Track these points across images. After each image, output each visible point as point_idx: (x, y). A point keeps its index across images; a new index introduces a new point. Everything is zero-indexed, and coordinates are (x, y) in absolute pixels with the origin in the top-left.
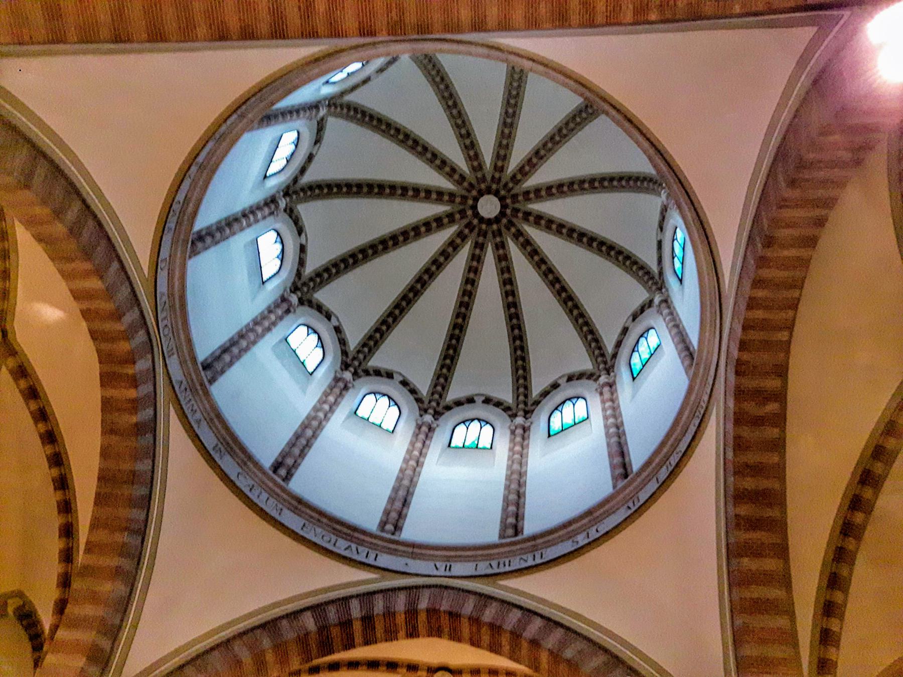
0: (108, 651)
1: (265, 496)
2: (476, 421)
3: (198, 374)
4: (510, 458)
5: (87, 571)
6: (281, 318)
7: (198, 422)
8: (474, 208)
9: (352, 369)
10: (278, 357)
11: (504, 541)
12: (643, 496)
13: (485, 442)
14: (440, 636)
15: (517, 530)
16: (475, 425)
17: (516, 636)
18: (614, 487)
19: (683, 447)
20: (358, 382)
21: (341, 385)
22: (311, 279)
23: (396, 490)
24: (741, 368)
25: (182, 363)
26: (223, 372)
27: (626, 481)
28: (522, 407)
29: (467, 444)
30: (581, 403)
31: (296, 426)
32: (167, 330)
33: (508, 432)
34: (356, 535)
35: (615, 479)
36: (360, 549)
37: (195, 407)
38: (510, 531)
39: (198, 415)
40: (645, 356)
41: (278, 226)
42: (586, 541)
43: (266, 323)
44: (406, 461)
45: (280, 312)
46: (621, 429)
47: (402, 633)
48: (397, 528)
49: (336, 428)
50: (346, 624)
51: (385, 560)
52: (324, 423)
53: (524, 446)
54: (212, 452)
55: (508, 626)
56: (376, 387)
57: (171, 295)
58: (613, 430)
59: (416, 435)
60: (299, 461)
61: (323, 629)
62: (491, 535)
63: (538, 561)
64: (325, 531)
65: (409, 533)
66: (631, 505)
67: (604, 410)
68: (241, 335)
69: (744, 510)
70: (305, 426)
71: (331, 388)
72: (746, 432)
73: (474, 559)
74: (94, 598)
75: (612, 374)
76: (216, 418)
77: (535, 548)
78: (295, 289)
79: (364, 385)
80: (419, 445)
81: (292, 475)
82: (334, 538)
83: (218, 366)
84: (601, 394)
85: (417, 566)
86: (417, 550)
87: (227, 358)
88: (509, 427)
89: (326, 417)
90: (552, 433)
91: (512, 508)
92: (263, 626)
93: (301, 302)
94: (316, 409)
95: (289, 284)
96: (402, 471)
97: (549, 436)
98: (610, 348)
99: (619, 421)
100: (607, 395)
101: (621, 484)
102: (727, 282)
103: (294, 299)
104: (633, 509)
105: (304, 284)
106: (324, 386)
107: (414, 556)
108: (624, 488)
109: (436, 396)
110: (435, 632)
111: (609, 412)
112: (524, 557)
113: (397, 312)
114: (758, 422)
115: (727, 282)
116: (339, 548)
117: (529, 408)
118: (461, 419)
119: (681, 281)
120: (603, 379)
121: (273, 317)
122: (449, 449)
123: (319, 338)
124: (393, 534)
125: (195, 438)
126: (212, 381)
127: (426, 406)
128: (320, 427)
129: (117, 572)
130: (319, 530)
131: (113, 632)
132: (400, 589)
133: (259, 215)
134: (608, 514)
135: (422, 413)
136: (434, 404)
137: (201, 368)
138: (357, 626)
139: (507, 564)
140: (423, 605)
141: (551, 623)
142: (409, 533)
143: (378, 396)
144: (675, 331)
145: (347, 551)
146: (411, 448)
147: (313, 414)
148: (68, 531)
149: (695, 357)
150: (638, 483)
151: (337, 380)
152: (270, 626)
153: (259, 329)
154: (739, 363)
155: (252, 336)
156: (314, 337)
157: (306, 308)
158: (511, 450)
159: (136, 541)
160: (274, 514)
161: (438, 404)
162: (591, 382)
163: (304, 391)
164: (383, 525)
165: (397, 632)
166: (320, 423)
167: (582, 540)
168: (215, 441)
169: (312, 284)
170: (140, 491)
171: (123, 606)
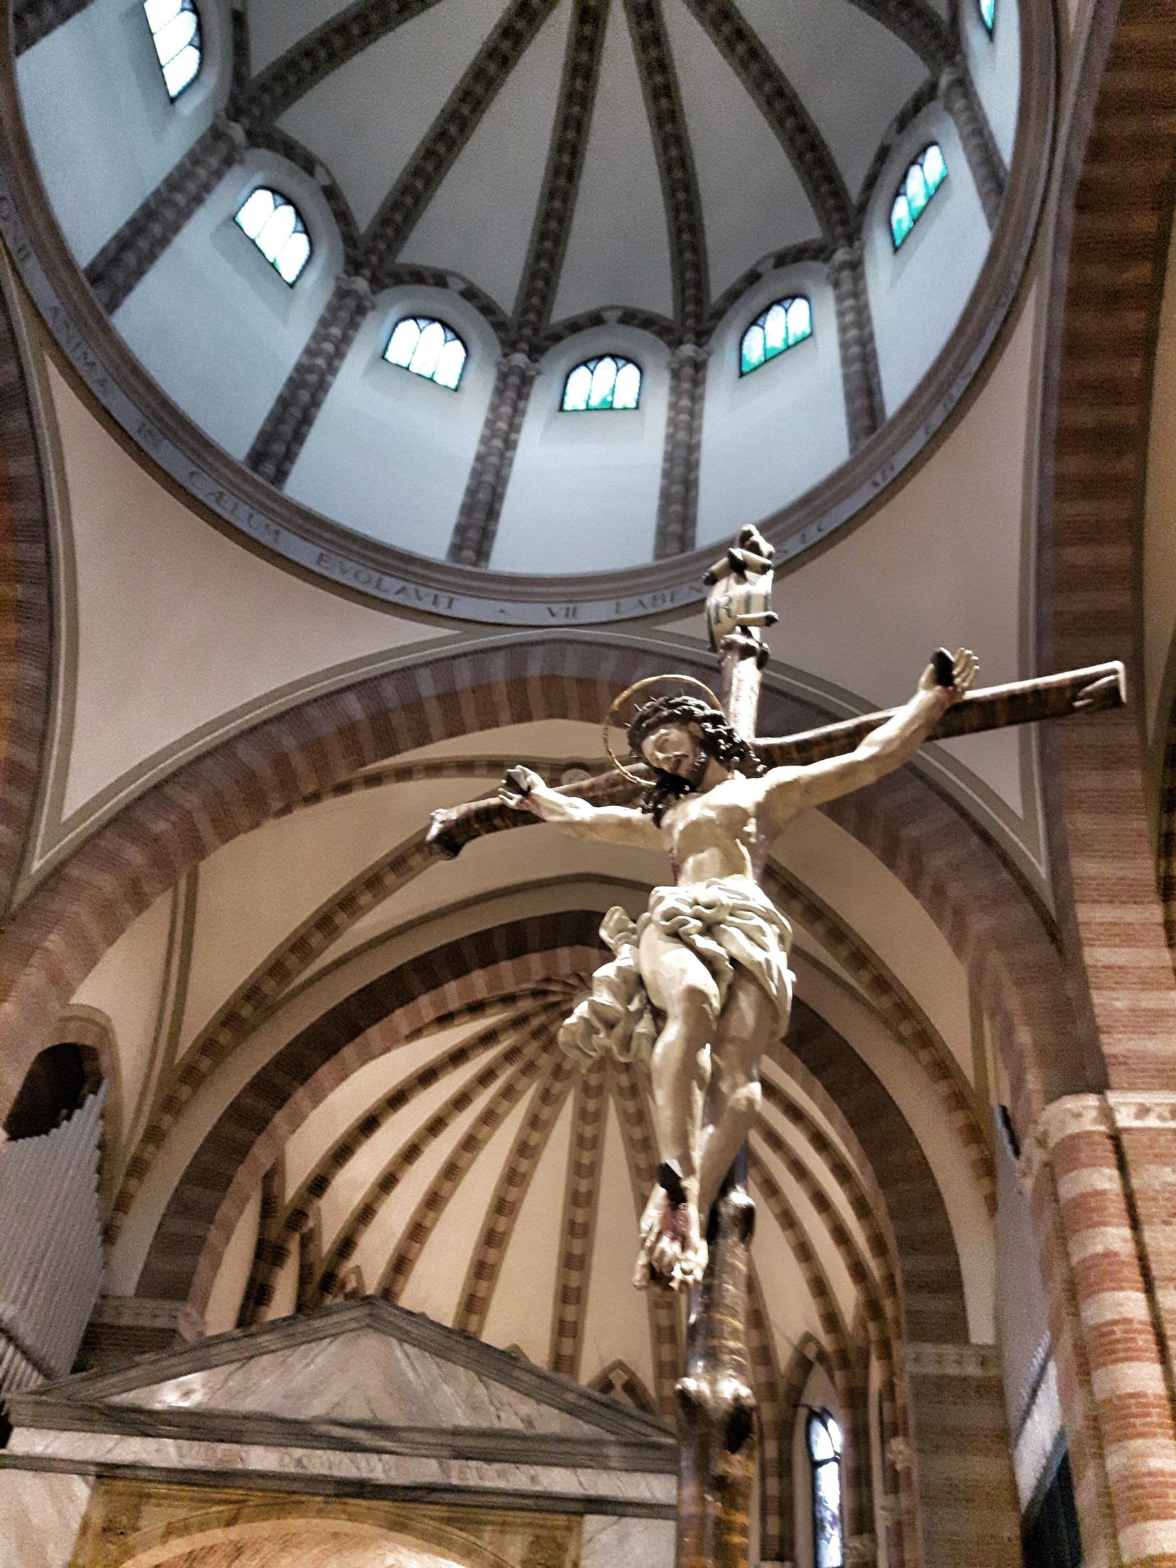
0: (35, 769)
3: (84, 293)
6: (218, 175)
9: (367, 272)
11: (661, 562)
12: (902, 460)
13: (626, 396)
14: (564, 716)
15: (685, 540)
16: (607, 364)
18: (853, 450)
20: (383, 296)
21: (350, 303)
22: (264, 88)
23: (471, 492)
24: (1088, 198)
25: (50, 272)
26: (128, 289)
27: (873, 436)
28: (689, 325)
29: (594, 403)
30: (800, 305)
34: (411, 568)
35: (855, 435)
36: (423, 591)
38: (674, 546)
40: (920, 202)
42: (801, 547)
43: (192, 187)
44: (485, 440)
45: (214, 162)
46: (869, 348)
47: (505, 715)
48: (483, 554)
50: (414, 706)
51: (466, 607)
53: (696, 398)
56: (418, 305)
58: (855, 350)
59: (499, 392)
62: (636, 548)
64: (351, 563)
66: (878, 477)
67: (840, 314)
69: (1075, 464)
75: (857, 244)
78: (235, 111)
79: (395, 302)
80: (506, 410)
82: (376, 576)
84: (836, 285)
85: (516, 612)
87: (130, 258)
88: (669, 365)
89: (332, 370)
91: (676, 508)
95: (222, 104)
96: (479, 458)
97: (742, 375)
98: (854, 185)
99: (866, 331)
100: (847, 286)
101: (866, 442)
103: (237, 132)
105: (253, 100)
107: (513, 598)
108: (870, 449)
109: (532, 316)
111: (849, 318)
113: (441, 149)
114: (1113, 299)
116: (386, 591)
117: (708, 325)
118: (577, 356)
119: (990, 33)
120: (841, 255)
121: (202, 172)
122: (561, 415)
123: (299, 214)
124: (475, 565)
126: (113, 305)
127: (513, 336)
128: (322, 387)
130: (349, 565)
131: (42, 740)
134: (848, 493)
135: (507, 351)
136: (527, 331)
137: (87, 285)
138: (433, 710)
139: (668, 599)
144: (975, 141)
145: (401, 595)
147: (306, 361)
149: (1006, 189)
151: (341, 294)
152: (293, 716)
154: (1085, 187)
155: (169, 214)
157: (264, 154)
160: (266, 539)
161: (536, 331)
162: (817, 265)
164: (456, 549)
168: (138, 416)
169: (266, 98)
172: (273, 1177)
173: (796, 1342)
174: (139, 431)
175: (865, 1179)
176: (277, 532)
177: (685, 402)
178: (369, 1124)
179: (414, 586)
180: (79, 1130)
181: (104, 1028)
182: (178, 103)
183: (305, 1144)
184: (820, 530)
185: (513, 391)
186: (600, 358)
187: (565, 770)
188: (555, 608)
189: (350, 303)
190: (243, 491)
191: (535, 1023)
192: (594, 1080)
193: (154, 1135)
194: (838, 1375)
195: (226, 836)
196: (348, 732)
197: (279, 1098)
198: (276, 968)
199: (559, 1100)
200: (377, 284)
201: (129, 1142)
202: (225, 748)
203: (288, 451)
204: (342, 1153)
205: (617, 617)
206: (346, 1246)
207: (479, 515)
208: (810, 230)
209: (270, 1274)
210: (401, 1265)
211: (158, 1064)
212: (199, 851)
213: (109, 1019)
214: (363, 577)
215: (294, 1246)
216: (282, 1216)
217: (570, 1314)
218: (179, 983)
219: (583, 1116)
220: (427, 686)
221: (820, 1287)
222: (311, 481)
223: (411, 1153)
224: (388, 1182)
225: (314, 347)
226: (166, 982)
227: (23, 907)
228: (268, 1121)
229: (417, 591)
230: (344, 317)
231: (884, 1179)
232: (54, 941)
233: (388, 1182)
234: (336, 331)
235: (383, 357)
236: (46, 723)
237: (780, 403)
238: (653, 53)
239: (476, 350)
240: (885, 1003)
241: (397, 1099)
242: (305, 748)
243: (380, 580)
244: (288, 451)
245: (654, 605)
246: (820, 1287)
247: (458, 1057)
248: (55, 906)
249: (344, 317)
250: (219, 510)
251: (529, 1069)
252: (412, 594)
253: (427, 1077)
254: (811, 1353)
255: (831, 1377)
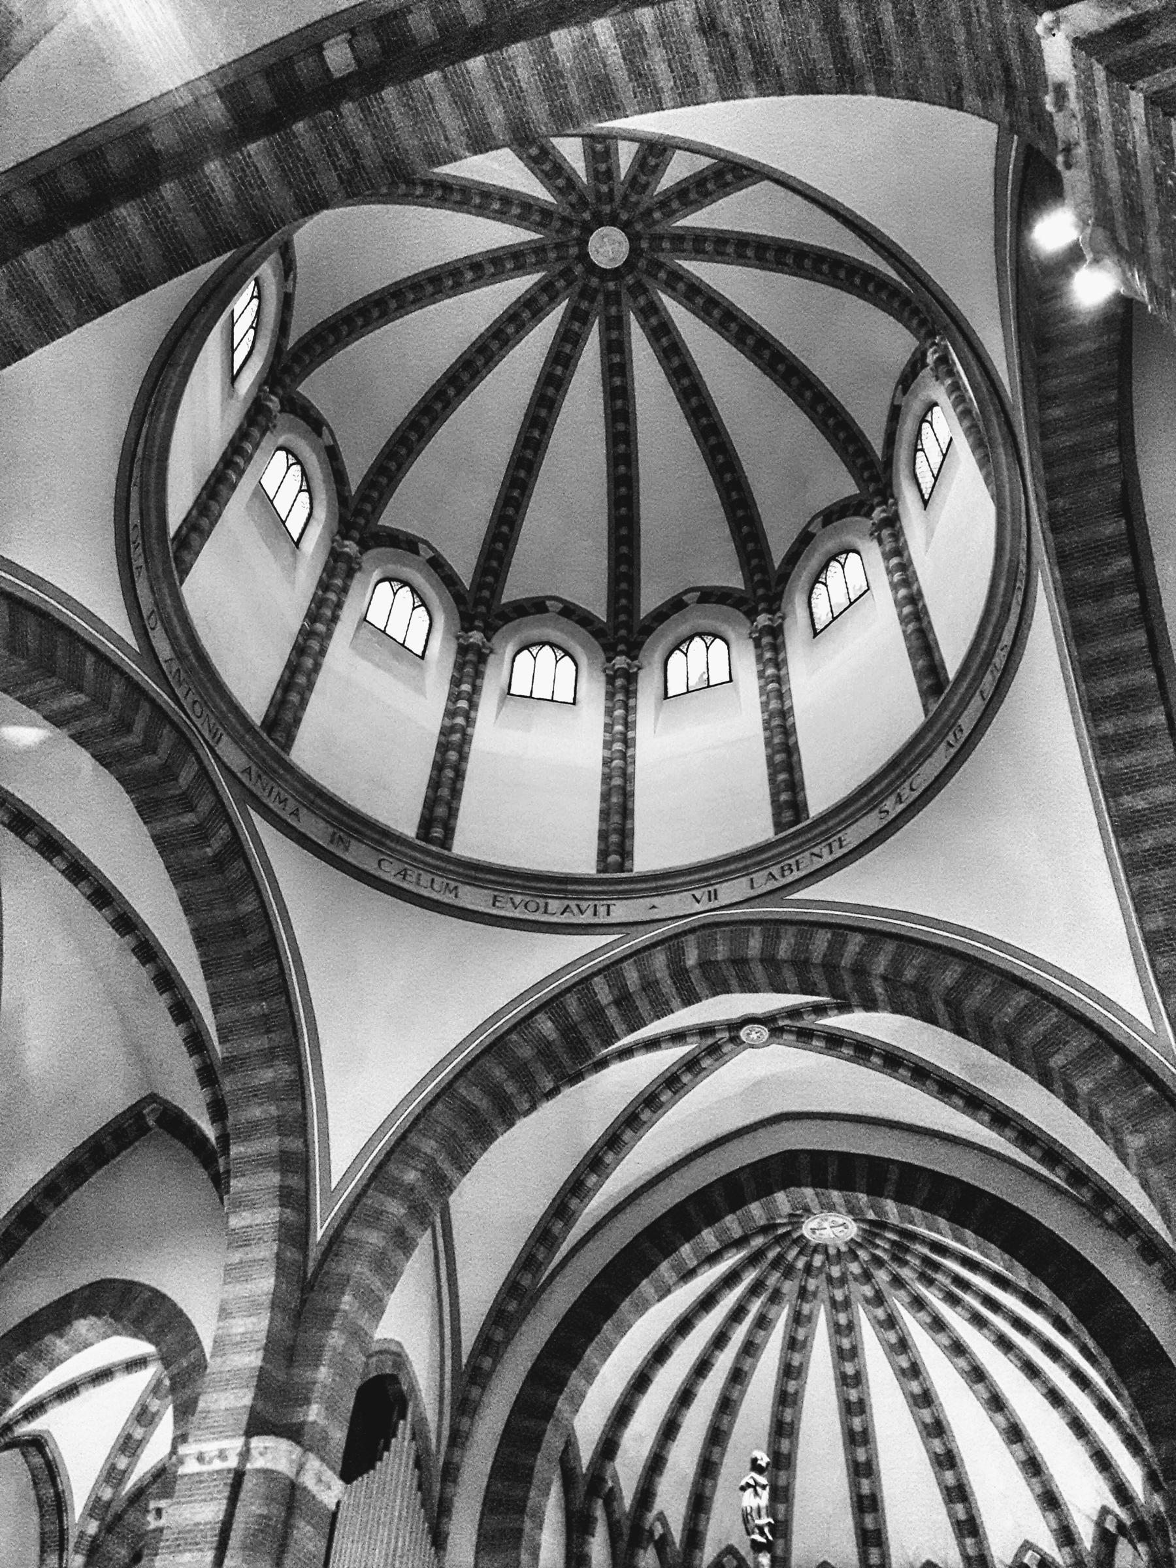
1: (426, 878)
2: (697, 639)
3: (262, 743)
4: (762, 689)
5: (233, 1064)
6: (345, 590)
7: (295, 813)
8: (584, 257)
10: (365, 656)
13: (719, 674)
16: (697, 644)
17: (830, 967)
18: (926, 711)
19: (1007, 638)
25: (237, 741)
26: (297, 721)
28: (761, 595)
31: (429, 753)
32: (197, 706)
33: (751, 643)
36: (584, 904)
37: (284, 795)
38: (788, 815)
39: (292, 804)
41: (281, 441)
42: (901, 807)
44: (607, 745)
49: (490, 733)
51: (621, 911)
52: (469, 730)
53: (779, 663)
54: (331, 848)
55: (817, 956)
57: (180, 656)
59: (610, 696)
60: (454, 805)
61: (568, 1030)
63: (838, 853)
64: (522, 896)
65: (644, 861)
68: (299, 650)
70: (443, 747)
71: (459, 666)
72: (1088, 612)
73: (745, 871)
74: (254, 1094)
76: (316, 797)
77: (826, 836)
80: (619, 712)
81: (453, 830)
82: (541, 902)
83: (288, 716)
84: (880, 542)
86: (662, 882)
87: (294, 698)
90: (819, 627)
92: (487, 1050)
93: (364, 547)
94: (450, 713)
95: (335, 526)
96: (606, 762)
102: (1008, 389)
104: (958, 746)
106: (448, 671)
107: (659, 892)
108: (938, 714)
110: (720, 987)
111: (897, 577)
112: (816, 850)
115: (1008, 389)
123: (414, 591)
125: (302, 840)
126: (288, 745)
128: (466, 739)
129: (269, 1057)
130: (518, 899)
131: (300, 1126)
132: (654, 945)
133: (249, 447)
134: (927, 754)
135: (611, 654)
138: (612, 1013)
139: (794, 867)
140: (692, 958)
141: (875, 936)
142: (644, 861)
143: (534, 650)
146: (609, 721)
147: (448, 723)
148: (182, 1011)
150: (959, 702)
151: (463, 650)
152: (497, 1047)
153: (320, 627)
156: (405, 592)
158: (761, 674)
159: (278, 1003)
160: (448, 898)
161: (630, 630)
163: (420, 690)
165: (667, 1003)
166: (464, 734)
167: (892, 807)
170: (257, 938)
171: (298, 1088)
172: (570, 1443)
173: (1095, 1518)
174: (332, 842)
175: (1020, 1276)
176: (456, 888)
177: (770, 671)
178: (641, 1382)
179: (576, 902)
180: (402, 1446)
181: (399, 1355)
182: (303, 545)
183: (588, 1421)
184: (912, 789)
185: (622, 689)
186: (690, 638)
187: (741, 1028)
188: (698, 894)
189: (471, 657)
190: (420, 863)
191: (771, 1255)
192: (839, 1295)
193: (458, 1439)
194: (1142, 1548)
195: (464, 1169)
196: (545, 1050)
197: (559, 1384)
198: (528, 1262)
199: (810, 1319)
200: (490, 631)
201: (438, 1452)
202: (447, 1090)
203: (450, 809)
204: (622, 1414)
205: (753, 893)
206: (645, 1495)
207: (616, 819)
208: (847, 487)
209: (584, 1543)
210: (699, 1504)
211: (448, 1376)
212: (442, 1186)
213: (399, 1344)
214: (532, 906)
215: (599, 1513)
216: (582, 1488)
217: (869, 1521)
218: (451, 1305)
219: (837, 1330)
220: (603, 993)
221: (1102, 1461)
222: (472, 840)
223: (685, 1397)
224: (670, 1429)
225: (452, 707)
226: (436, 1257)
227: (315, 1274)
228: (553, 1407)
229: (578, 906)
230: (470, 665)
231: (1035, 1269)
232: (347, 1301)
233: (670, 1429)
234: (466, 687)
235: (509, 693)
236: (304, 1107)
237: (852, 680)
238: (681, 286)
239: (583, 661)
240: (1086, 1195)
241: (661, 1353)
242: (513, 1075)
243: (547, 904)
244: (450, 809)
245: (783, 876)
246: (1102, 1461)
247: (707, 1302)
248: (342, 1269)
249: (470, 665)
250: (405, 885)
251: (776, 1297)
252: (576, 911)
253: (684, 1326)
254: (1110, 1526)
255: (1136, 1548)
